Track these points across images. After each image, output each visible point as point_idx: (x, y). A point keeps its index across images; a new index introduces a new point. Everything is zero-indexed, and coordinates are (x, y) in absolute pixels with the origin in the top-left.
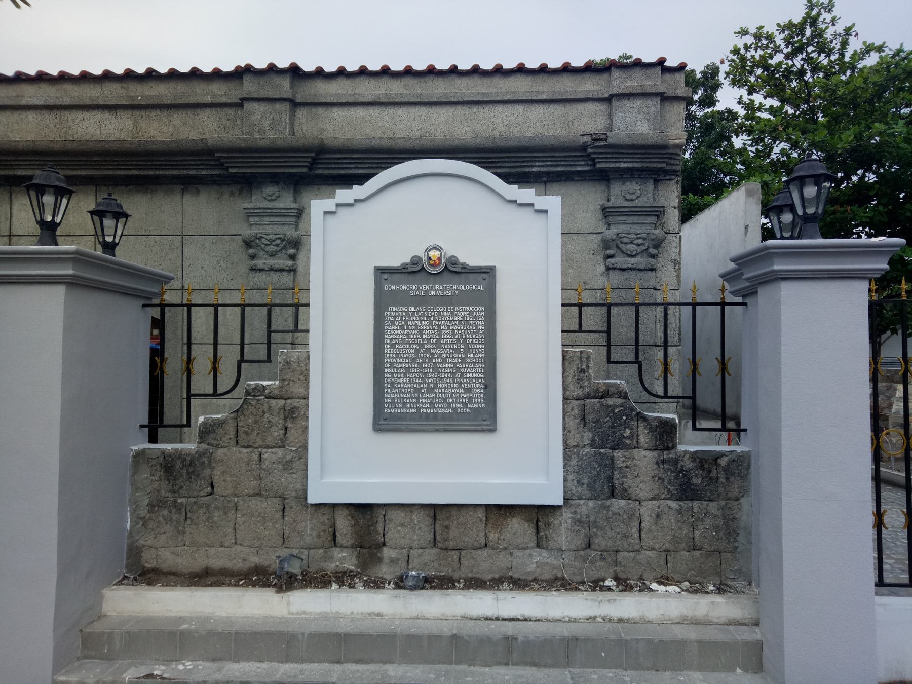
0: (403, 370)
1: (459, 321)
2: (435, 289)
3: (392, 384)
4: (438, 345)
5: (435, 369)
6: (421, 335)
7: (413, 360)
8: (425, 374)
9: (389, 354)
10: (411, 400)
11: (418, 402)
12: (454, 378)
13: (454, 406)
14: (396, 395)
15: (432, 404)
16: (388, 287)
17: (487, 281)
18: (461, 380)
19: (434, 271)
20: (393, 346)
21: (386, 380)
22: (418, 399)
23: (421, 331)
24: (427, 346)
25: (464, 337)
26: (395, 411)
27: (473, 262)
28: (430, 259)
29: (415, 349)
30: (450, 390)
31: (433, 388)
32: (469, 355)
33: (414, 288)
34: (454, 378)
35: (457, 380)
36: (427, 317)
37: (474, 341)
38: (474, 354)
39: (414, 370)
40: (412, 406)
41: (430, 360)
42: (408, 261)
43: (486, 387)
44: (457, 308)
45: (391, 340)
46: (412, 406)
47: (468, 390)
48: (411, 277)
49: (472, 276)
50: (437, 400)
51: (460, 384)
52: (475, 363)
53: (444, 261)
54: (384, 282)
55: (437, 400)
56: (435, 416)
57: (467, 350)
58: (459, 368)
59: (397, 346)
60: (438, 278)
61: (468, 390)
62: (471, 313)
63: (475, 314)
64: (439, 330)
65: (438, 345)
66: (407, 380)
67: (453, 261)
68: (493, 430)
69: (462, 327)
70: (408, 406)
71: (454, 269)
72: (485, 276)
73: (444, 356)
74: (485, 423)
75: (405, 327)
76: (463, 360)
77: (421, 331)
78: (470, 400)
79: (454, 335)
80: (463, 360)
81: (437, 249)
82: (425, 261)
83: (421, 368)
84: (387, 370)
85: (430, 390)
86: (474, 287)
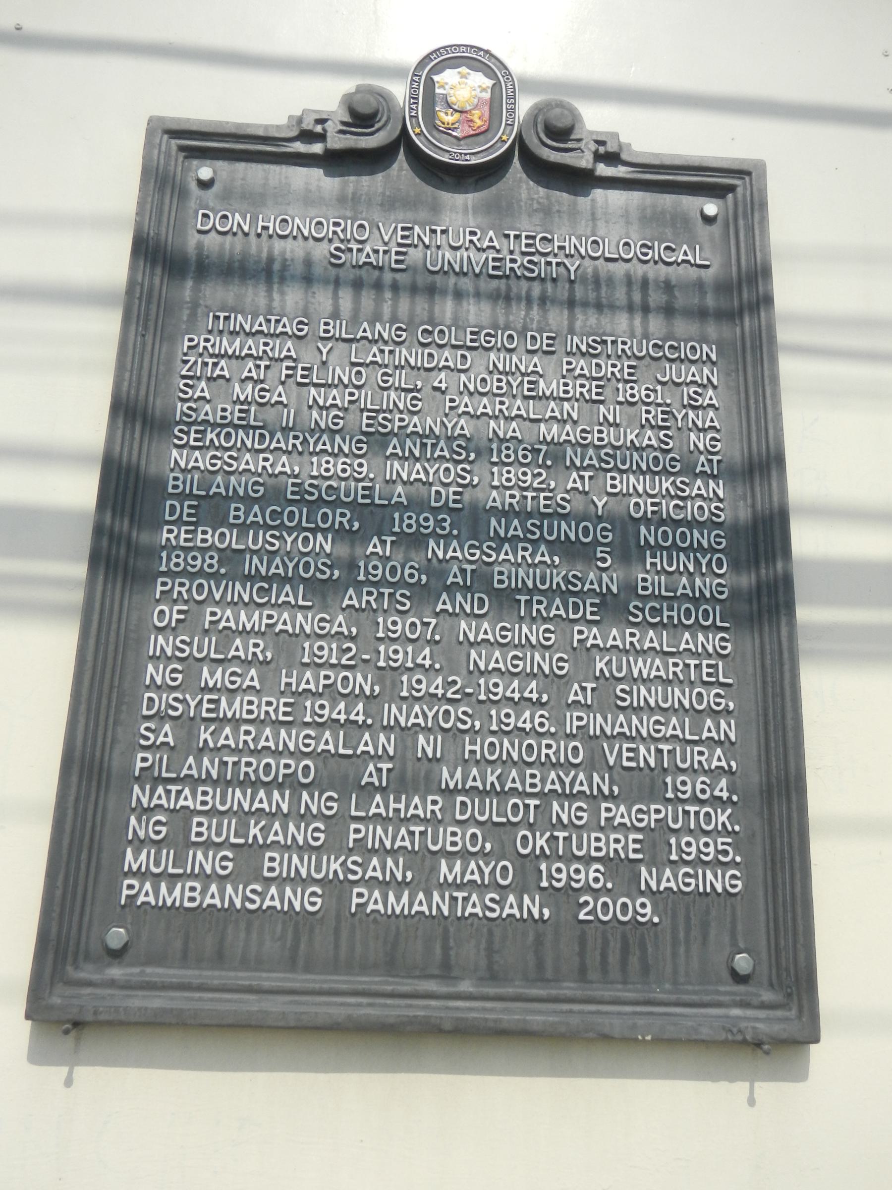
3: (187, 724)
8: (389, 675)
10: (297, 833)
11: (335, 844)
13: (561, 874)
15: (423, 862)
21: (153, 701)
22: (336, 824)
39: (330, 652)
40: (302, 866)
46: (302, 866)
47: (645, 785)
50: (448, 838)
55: (448, 838)
61: (645, 785)
68: (761, 166)
70: (273, 863)
71: (550, 157)
84: (161, 643)
85: (412, 776)
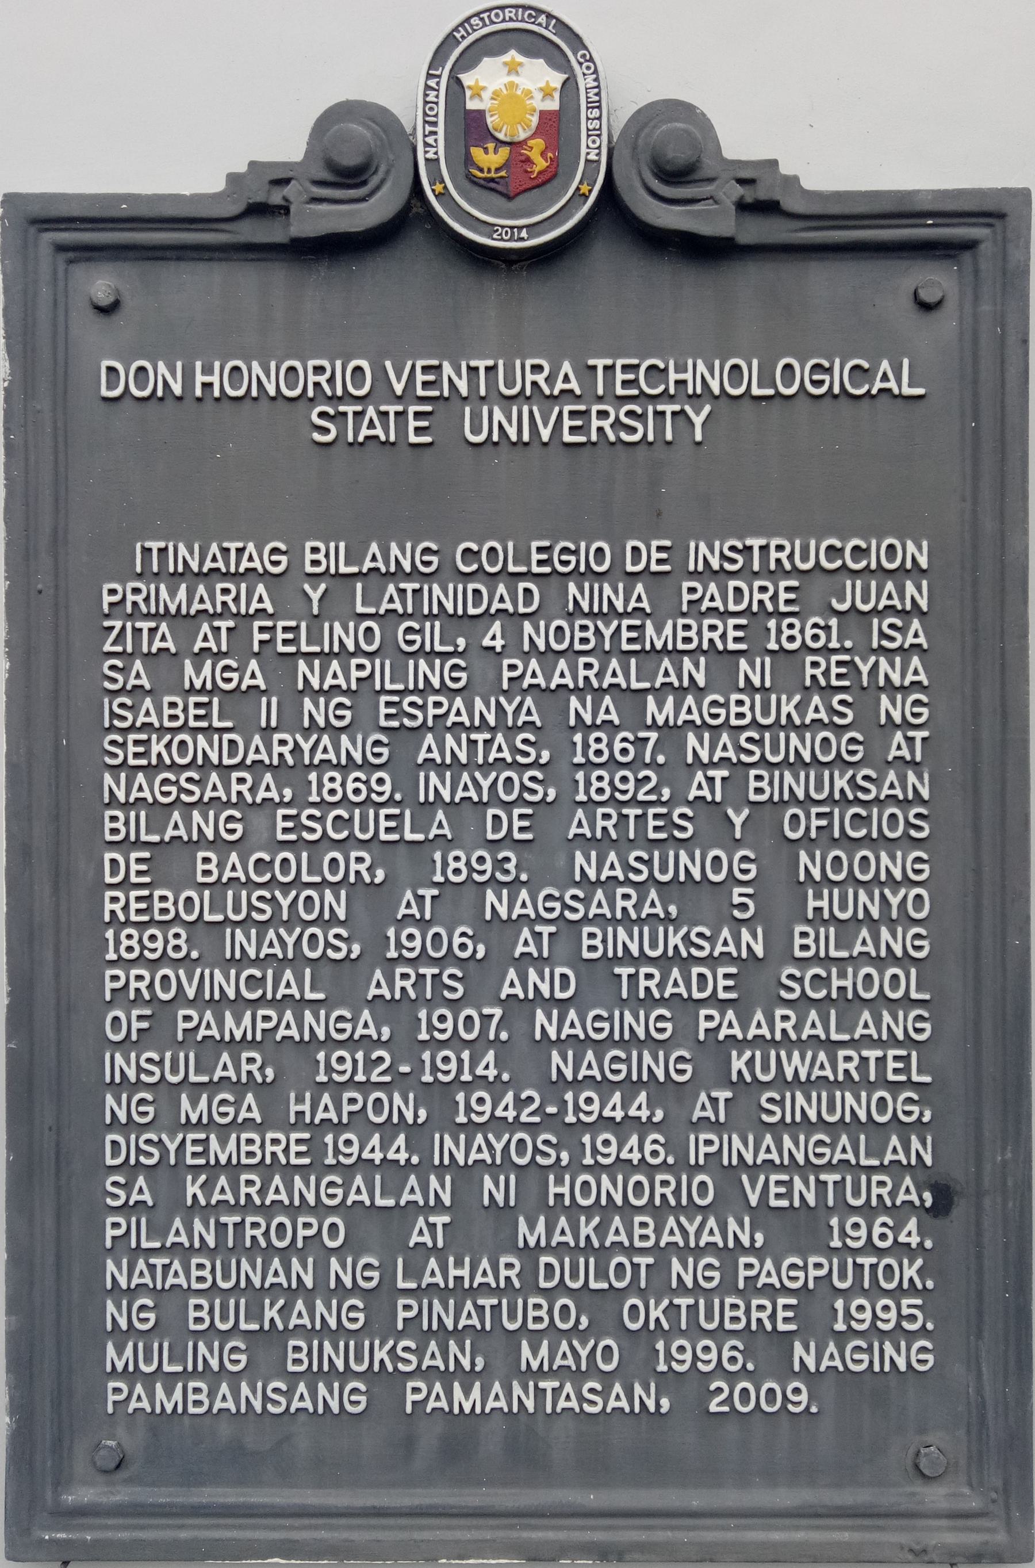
0: (252, 1064)
1: (722, 659)
2: (520, 382)
3: (168, 1174)
4: (542, 852)
5: (524, 1055)
6: (405, 769)
7: (341, 979)
8: (439, 1095)
9: (136, 944)
11: (378, 1322)
12: (676, 1130)
14: (202, 1271)
16: (115, 371)
17: (947, 324)
18: (737, 1147)
19: (508, 230)
20: (169, 860)
21: (115, 1149)
23: (404, 737)
24: (455, 865)
25: (760, 787)
26: (195, 1398)
27: (833, 158)
28: (471, 128)
29: (356, 888)
30: (644, 1227)
31: (503, 1215)
32: (803, 939)
33: (341, 369)
34: (676, 1130)
35: (700, 1146)
36: (455, 622)
37: (842, 820)
38: (846, 929)
39: (346, 1064)
41: (480, 977)
42: (289, 146)
43: (942, 1206)
44: (702, 553)
45: (159, 812)
47: (799, 1228)
48: (319, 290)
49: (823, 282)
50: (536, 1310)
51: (730, 1175)
52: (848, 1005)
53: (590, 149)
54: (86, 328)
55: (536, 1310)
56: (525, 1443)
57: (782, 898)
58: (717, 1050)
59: (206, 864)
60: (538, 299)
61: (799, 1228)
62: (813, 586)
63: (852, 595)
64: (554, 729)
65: (542, 852)
66: (288, 1145)
67: (673, 150)
68: (1030, 1560)
69: (741, 708)
72: (935, 279)
73: (592, 944)
74: (936, 1496)
75: (268, 711)
76: (754, 983)
77: (404, 737)
78: (813, 1304)
79: (678, 769)
80: (754, 983)
81: (534, 45)
82: (433, 147)
83: (407, 1045)
85: (482, 1227)
86: (839, 377)
